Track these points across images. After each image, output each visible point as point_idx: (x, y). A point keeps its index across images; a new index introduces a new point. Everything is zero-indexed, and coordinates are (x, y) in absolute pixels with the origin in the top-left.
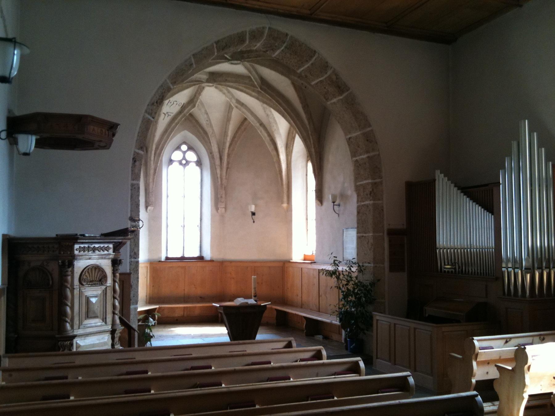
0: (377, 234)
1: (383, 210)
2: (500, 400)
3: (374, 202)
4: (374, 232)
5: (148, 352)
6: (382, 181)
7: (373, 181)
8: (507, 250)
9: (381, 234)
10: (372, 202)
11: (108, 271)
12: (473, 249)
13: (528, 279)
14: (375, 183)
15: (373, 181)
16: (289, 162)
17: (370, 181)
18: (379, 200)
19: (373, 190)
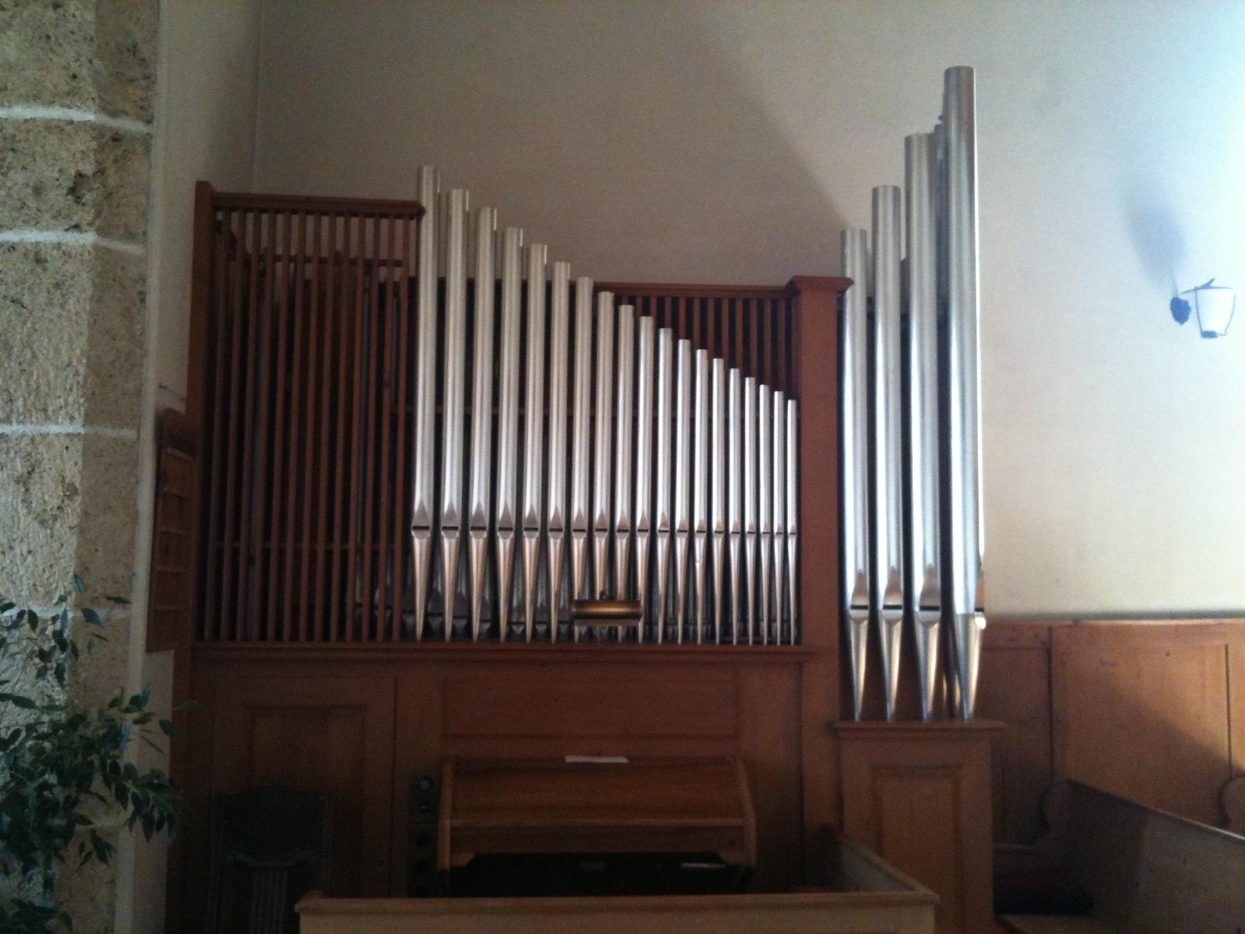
0: (109, 432)
1: (142, 296)
2: (898, 262)
3: (104, 242)
4: (88, 420)
5: (803, 569)
6: (150, 136)
7: (105, 120)
8: (632, 560)
9: (128, 433)
10: (88, 238)
11: (51, 672)
12: (465, 529)
13: (762, 597)
14: (117, 138)
15: (105, 120)
16: (672, 553)
17: (90, 117)
18: (130, 236)
19: (100, 172)
